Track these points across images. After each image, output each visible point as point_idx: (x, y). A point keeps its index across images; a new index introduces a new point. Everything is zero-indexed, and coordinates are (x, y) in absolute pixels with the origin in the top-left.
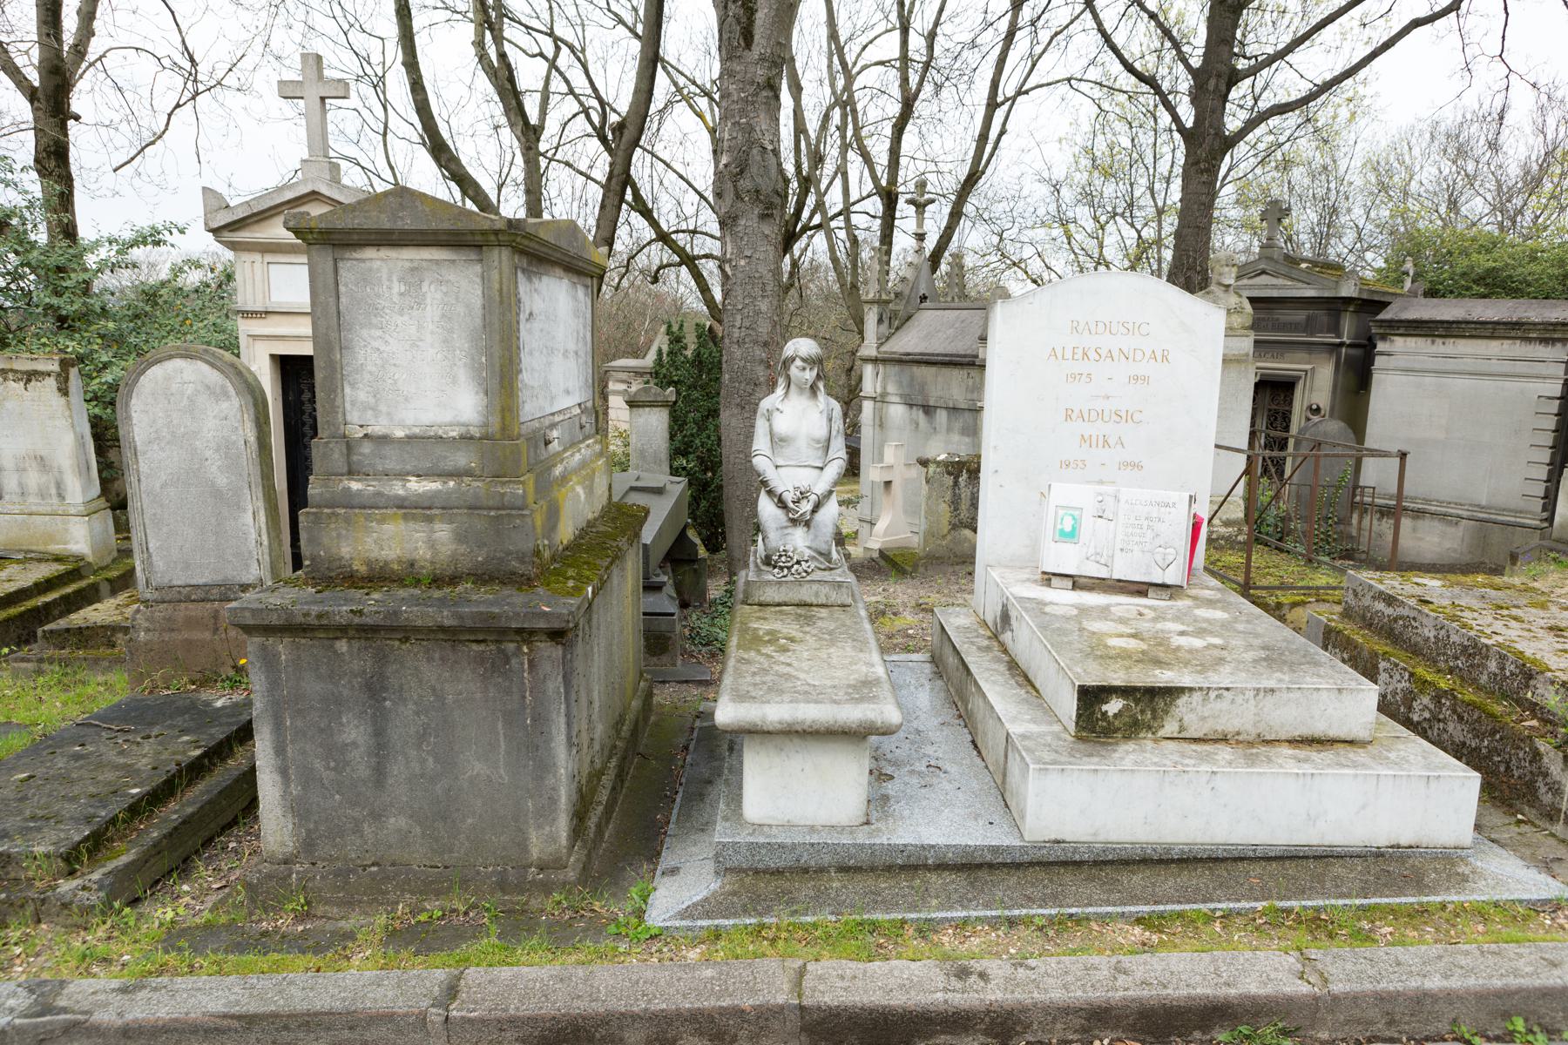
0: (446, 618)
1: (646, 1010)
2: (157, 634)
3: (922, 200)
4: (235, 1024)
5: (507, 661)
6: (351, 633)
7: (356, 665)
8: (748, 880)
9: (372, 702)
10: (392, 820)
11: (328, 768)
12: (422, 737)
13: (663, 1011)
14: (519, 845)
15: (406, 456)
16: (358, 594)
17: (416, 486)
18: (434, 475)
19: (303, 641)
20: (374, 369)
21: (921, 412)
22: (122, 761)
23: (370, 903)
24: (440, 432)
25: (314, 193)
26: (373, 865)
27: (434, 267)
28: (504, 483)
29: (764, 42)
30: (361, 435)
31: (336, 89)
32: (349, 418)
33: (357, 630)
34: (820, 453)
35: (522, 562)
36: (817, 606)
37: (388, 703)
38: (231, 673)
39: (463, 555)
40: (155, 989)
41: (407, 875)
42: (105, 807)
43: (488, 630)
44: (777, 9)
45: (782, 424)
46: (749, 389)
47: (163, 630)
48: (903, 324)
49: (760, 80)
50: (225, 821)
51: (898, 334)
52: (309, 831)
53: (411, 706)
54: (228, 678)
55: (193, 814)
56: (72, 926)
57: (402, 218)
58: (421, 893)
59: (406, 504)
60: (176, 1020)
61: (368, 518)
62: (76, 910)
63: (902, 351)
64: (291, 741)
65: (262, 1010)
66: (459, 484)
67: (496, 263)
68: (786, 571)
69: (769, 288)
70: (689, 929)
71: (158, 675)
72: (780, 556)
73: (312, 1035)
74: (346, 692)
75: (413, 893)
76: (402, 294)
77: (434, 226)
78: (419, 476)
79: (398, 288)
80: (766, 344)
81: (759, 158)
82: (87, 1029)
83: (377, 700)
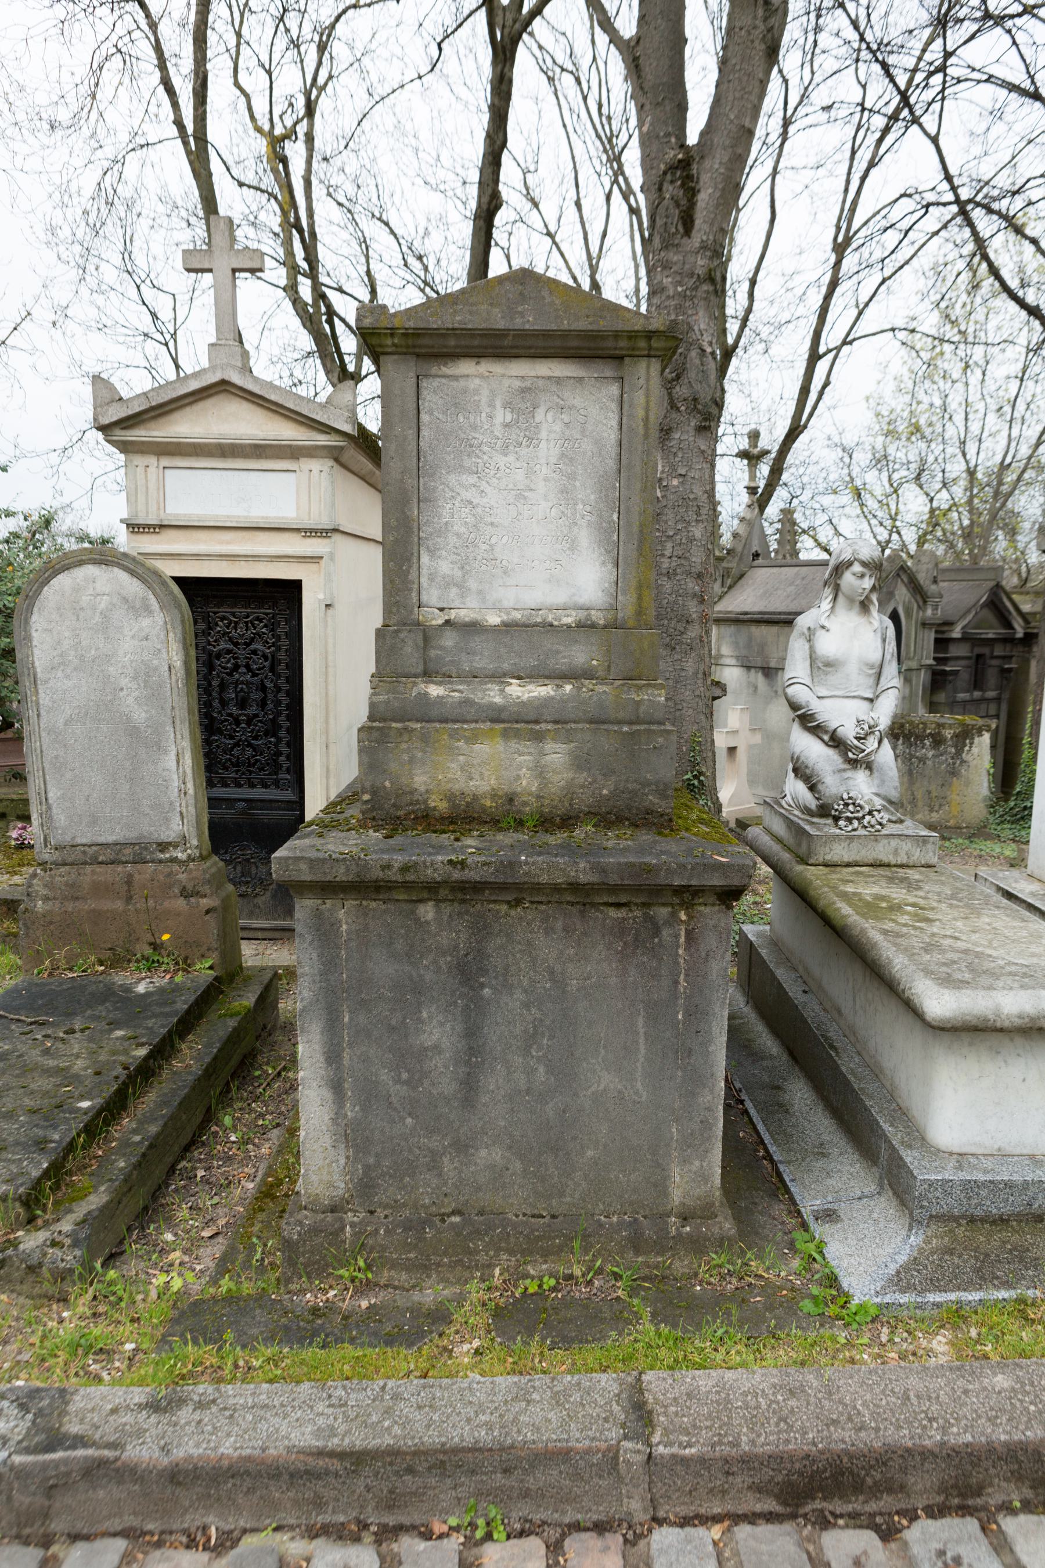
0: (583, 872)
1: (943, 1444)
2: (58, 904)
3: (756, 451)
4: (336, 1465)
5: (657, 931)
6: (443, 893)
7: (445, 939)
8: (960, 1232)
9: (465, 990)
10: (484, 1152)
11: (398, 1081)
12: (531, 1038)
13: (967, 1445)
14: (656, 1186)
15: (503, 650)
16: (446, 839)
17: (517, 691)
18: (540, 676)
19: (373, 904)
20: (463, 530)
21: (760, 675)
22: (52, 1063)
23: (452, 1266)
24: (550, 618)
25: (224, 382)
26: (453, 1213)
27: (554, 388)
28: (640, 688)
29: (706, 227)
30: (440, 622)
31: (251, 259)
32: (424, 598)
33: (453, 889)
34: (871, 681)
35: (663, 796)
36: (896, 866)
37: (487, 991)
38: (148, 951)
39: (582, 786)
40: (200, 1406)
41: (504, 1228)
42: (55, 1127)
43: (637, 889)
44: (723, 189)
45: (828, 645)
46: (680, 627)
47: (65, 898)
48: (735, 583)
49: (700, 271)
50: (186, 1142)
51: (733, 592)
52: (367, 1168)
53: (518, 995)
54: (143, 957)
55: (158, 1135)
56: (40, 1296)
57: (522, 314)
58: (523, 1253)
59: (503, 716)
60: (249, 1459)
61: (454, 735)
62: (48, 1275)
63: (738, 610)
64: (350, 1045)
65: (374, 1443)
66: (579, 689)
67: (642, 381)
68: (856, 823)
69: (704, 511)
70: (919, 1306)
71: (60, 955)
72: (846, 805)
73: (448, 1481)
74: (429, 976)
75: (511, 1252)
76: (507, 425)
77: (565, 325)
78: (519, 678)
79: (502, 416)
80: (699, 576)
81: (698, 361)
82: (117, 1470)
83: (472, 988)
